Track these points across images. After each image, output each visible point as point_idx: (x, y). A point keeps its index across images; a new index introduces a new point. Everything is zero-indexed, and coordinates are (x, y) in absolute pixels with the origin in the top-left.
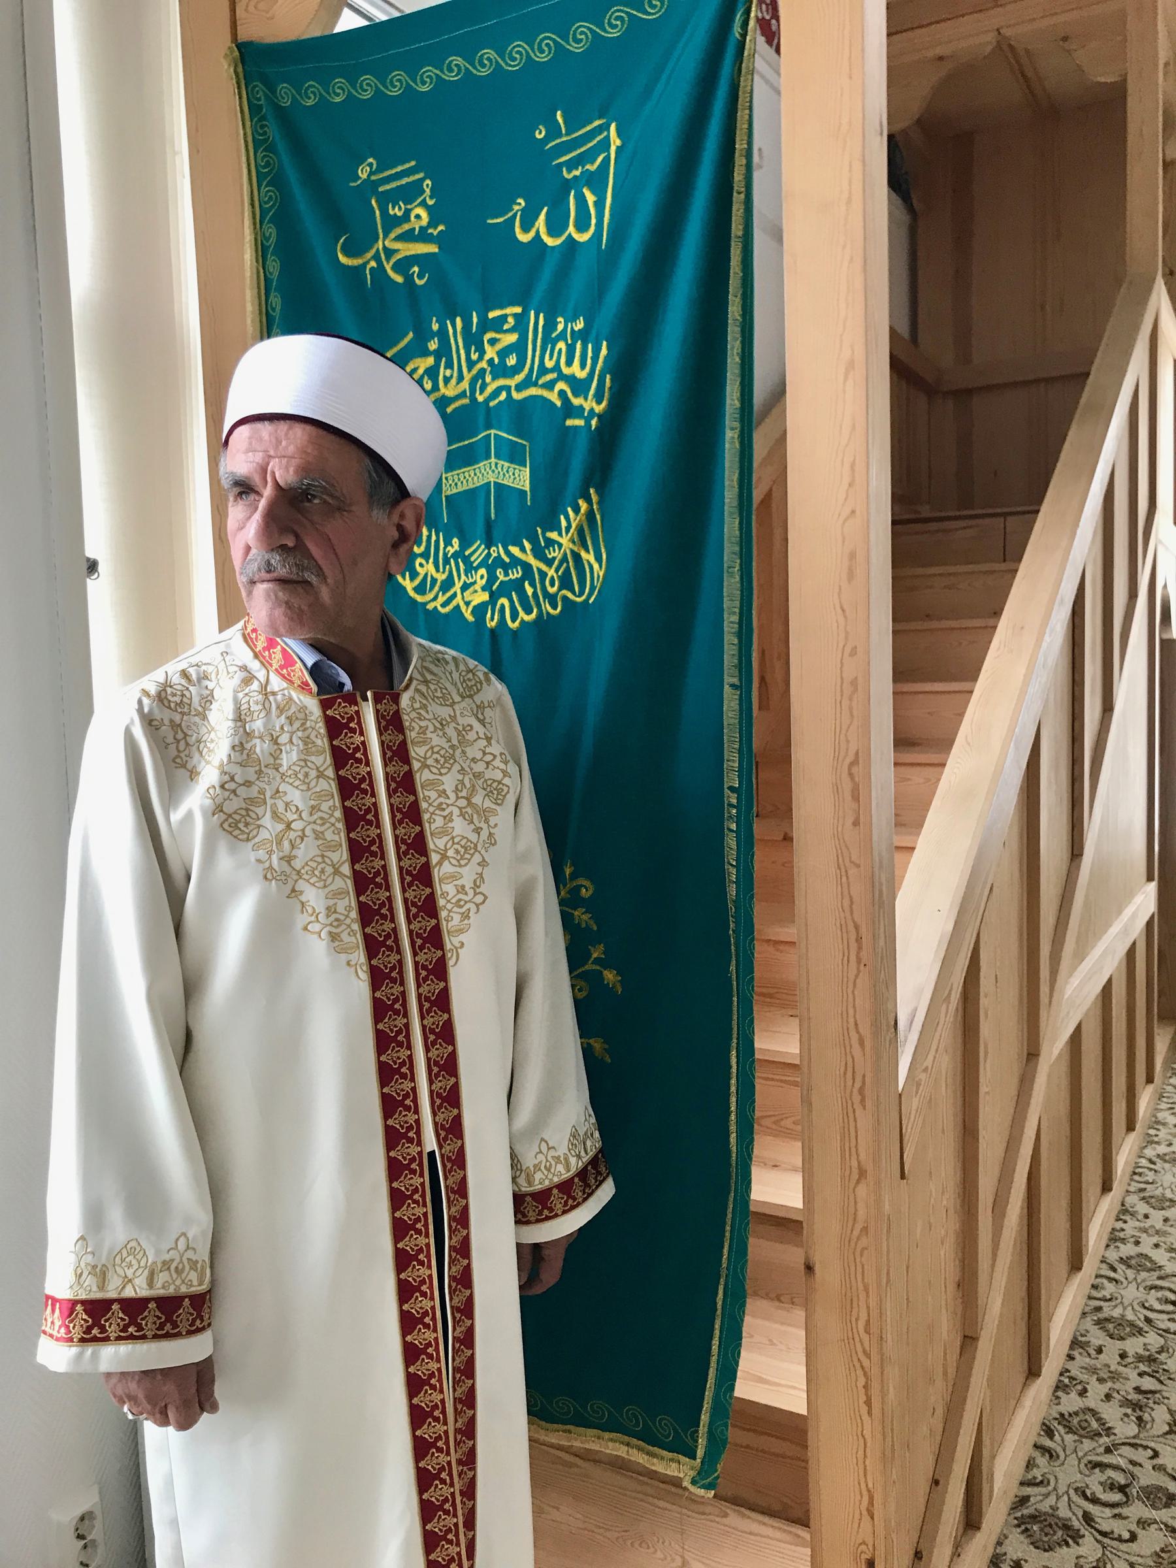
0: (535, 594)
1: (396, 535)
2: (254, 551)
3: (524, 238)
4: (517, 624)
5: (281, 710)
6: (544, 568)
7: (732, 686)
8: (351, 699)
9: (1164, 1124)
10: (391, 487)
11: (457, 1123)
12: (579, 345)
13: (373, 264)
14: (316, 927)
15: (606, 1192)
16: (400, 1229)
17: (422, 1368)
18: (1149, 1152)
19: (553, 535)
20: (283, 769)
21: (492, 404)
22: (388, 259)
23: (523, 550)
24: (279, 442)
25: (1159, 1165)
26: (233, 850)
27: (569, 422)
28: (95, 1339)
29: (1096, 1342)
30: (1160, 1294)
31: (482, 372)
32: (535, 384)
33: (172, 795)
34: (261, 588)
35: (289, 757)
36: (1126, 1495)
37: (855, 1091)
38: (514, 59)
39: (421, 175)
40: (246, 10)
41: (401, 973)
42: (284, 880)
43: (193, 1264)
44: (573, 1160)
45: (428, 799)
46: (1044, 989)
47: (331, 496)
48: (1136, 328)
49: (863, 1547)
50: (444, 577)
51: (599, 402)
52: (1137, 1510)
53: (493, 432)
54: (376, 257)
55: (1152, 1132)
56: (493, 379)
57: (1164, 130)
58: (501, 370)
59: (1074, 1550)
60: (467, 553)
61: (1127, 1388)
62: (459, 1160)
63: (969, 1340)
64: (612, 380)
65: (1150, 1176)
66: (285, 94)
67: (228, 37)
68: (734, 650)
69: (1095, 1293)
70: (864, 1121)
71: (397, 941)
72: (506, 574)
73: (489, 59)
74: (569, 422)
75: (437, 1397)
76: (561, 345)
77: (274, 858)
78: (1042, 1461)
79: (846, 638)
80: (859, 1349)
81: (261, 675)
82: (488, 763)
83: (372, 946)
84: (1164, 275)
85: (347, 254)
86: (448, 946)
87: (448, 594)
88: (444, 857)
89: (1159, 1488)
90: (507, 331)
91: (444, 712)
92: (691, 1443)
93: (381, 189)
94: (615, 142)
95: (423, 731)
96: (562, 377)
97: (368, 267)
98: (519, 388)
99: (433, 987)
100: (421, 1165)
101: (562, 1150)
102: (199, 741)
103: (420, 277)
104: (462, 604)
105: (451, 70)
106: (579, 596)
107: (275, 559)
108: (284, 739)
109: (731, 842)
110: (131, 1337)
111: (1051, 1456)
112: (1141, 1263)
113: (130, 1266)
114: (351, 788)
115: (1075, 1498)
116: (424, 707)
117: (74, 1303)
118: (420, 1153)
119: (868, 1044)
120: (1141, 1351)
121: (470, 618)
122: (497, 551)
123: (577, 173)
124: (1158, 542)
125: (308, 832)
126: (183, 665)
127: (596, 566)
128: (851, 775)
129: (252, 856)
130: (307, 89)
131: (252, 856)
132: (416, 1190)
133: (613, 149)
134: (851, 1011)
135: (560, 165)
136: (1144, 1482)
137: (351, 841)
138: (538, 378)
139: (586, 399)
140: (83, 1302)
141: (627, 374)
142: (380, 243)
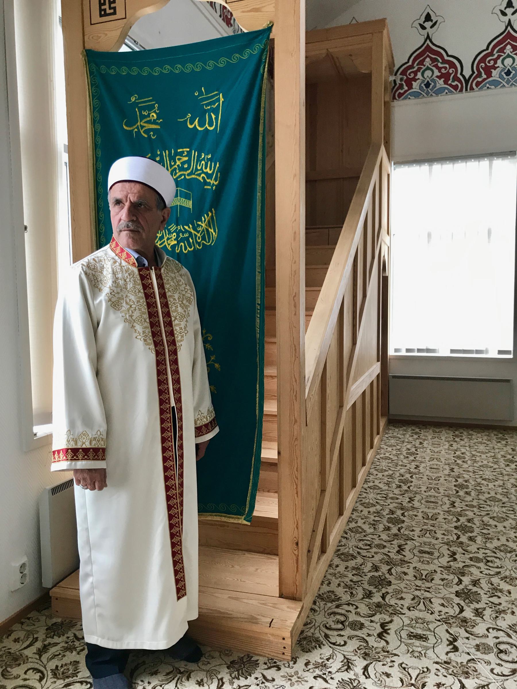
0: (193, 242)
1: (162, 218)
2: (122, 222)
3: (191, 127)
5: (126, 271)
7: (259, 272)
8: (147, 269)
9: (383, 449)
10: (163, 204)
11: (180, 398)
12: (209, 163)
13: (136, 130)
14: (139, 337)
15: (217, 430)
16: (163, 430)
17: (169, 473)
18: (378, 457)
19: (200, 223)
20: (128, 289)
23: (189, 227)
24: (131, 189)
26: (114, 313)
27: (206, 187)
28: (75, 459)
29: (361, 509)
32: (194, 174)
33: (94, 296)
34: (124, 233)
35: (130, 286)
39: (154, 102)
40: (89, 38)
41: (164, 352)
42: (130, 322)
43: (102, 439)
44: (208, 418)
45: (171, 301)
47: (148, 206)
48: (375, 164)
49: (295, 539)
51: (216, 181)
52: (374, 550)
54: (137, 128)
55: (379, 451)
57: (384, 90)
58: (181, 169)
59: (355, 561)
61: (371, 520)
62: (180, 410)
63: (323, 491)
66: (103, 69)
67: (82, 46)
68: (259, 261)
69: (360, 496)
70: (297, 407)
71: (163, 343)
72: (183, 235)
74: (206, 187)
75: (173, 482)
76: (203, 162)
77: (127, 316)
78: (344, 540)
80: (294, 477)
81: (119, 261)
82: (186, 292)
83: (156, 344)
84: (384, 144)
85: (126, 126)
86: (177, 345)
87: (162, 241)
88: (176, 319)
89: (381, 544)
90: (184, 156)
91: (173, 275)
94: (222, 100)
95: (168, 280)
96: (203, 172)
98: (188, 175)
99: (173, 357)
100: (170, 411)
101: (205, 414)
102: (101, 280)
103: (153, 136)
104: (167, 245)
107: (130, 224)
108: (128, 280)
109: (258, 321)
110: (86, 459)
112: (375, 487)
113: (84, 439)
114: (149, 296)
115: (355, 549)
116: (167, 273)
117: (67, 450)
118: (170, 407)
119: (298, 381)
120: (375, 510)
121: (170, 249)
124: (382, 240)
125: (137, 308)
126: (93, 257)
127: (214, 233)
128: (294, 300)
129: (121, 315)
131: (121, 315)
132: (168, 418)
134: (293, 372)
136: (376, 543)
137: (149, 312)
139: (211, 180)
140: (71, 449)
141: (225, 173)
142: (139, 123)
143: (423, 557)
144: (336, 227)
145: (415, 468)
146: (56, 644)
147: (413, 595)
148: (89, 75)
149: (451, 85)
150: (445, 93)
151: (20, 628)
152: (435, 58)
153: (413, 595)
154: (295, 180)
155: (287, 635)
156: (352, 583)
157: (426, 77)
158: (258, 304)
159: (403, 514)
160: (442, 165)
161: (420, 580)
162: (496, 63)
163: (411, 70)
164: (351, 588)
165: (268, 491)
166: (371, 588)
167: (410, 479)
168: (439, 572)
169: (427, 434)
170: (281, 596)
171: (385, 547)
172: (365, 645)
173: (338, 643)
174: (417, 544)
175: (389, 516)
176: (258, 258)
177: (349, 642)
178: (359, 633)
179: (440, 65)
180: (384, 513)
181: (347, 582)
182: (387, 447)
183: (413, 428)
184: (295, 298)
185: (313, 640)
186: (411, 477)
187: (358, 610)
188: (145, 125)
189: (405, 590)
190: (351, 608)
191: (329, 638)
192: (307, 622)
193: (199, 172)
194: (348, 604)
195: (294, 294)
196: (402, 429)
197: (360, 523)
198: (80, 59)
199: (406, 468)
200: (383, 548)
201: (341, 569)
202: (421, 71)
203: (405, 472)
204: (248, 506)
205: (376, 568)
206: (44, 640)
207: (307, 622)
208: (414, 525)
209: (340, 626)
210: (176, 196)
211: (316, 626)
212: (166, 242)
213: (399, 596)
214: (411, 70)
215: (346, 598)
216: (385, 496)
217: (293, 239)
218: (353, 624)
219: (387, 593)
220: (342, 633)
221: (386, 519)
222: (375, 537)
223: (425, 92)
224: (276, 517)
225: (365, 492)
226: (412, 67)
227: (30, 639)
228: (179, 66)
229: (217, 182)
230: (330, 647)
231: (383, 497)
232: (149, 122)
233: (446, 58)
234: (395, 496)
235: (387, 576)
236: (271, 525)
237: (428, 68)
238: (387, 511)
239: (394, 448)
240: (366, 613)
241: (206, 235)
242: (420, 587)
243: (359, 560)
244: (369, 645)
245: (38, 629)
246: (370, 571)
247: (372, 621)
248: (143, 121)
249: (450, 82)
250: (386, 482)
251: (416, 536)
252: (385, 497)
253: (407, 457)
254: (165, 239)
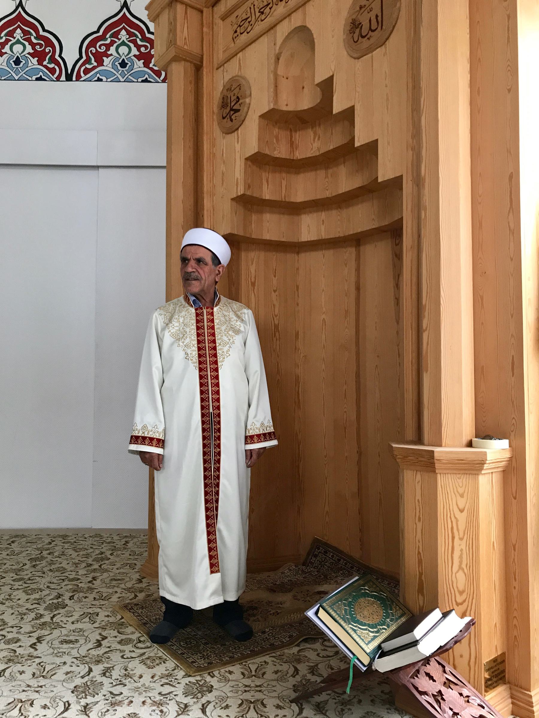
15: (274, 442)
86: (219, 365)
149: (46, 67)
157: (121, 54)
162: (108, 49)
166: (188, 700)
168: (270, 663)
179: (140, 43)
223: (120, 73)
226: (103, 38)
233: (42, 33)
249: (45, 63)
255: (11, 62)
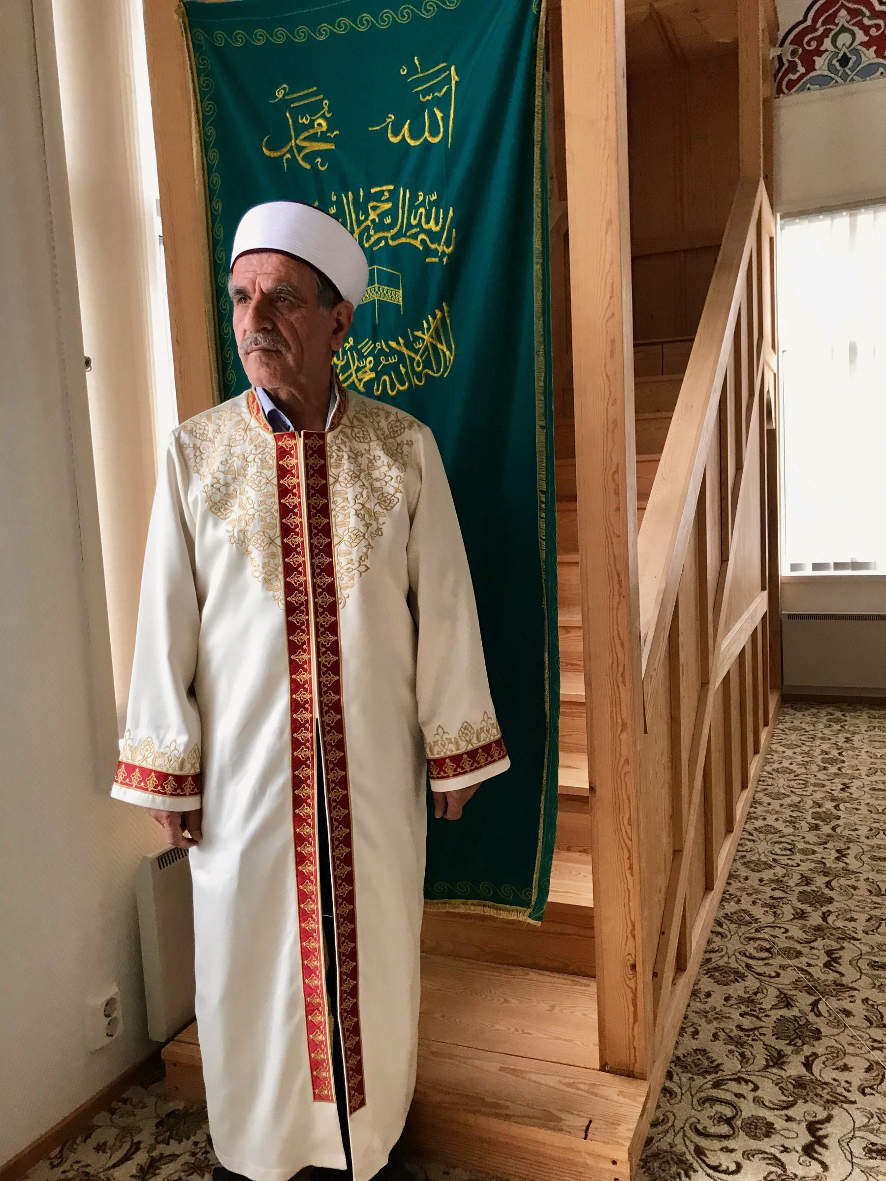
0: (407, 372)
1: (335, 325)
2: (248, 332)
3: (394, 140)
4: (394, 392)
6: (412, 355)
7: (541, 427)
9: (776, 752)
10: (331, 295)
12: (434, 211)
13: (288, 156)
18: (768, 768)
19: (419, 334)
21: (374, 249)
22: (299, 153)
25: (775, 775)
27: (428, 260)
29: (744, 874)
30: (781, 846)
31: (368, 228)
32: (405, 236)
36: (771, 953)
37: (619, 675)
38: (384, 21)
39: (321, 97)
46: (711, 642)
49: (629, 957)
50: (343, 363)
51: (448, 247)
52: (779, 960)
53: (375, 267)
55: (769, 756)
56: (375, 233)
58: (380, 226)
60: (359, 347)
63: (677, 852)
64: (456, 233)
65: (770, 782)
66: (220, 38)
69: (740, 848)
72: (387, 360)
73: (366, 20)
74: (428, 260)
76: (422, 210)
78: (717, 939)
79: (610, 394)
85: (269, 149)
87: (346, 375)
89: (790, 948)
90: (383, 201)
92: (525, 898)
93: (292, 106)
94: (455, 78)
96: (423, 231)
97: (285, 158)
98: (393, 238)
103: (322, 165)
104: (356, 381)
105: (340, 27)
106: (437, 373)
107: (260, 337)
109: (542, 524)
111: (722, 936)
112: (769, 830)
115: (740, 957)
122: (381, 345)
123: (429, 98)
124: (765, 361)
127: (448, 353)
128: (614, 480)
130: (237, 34)
133: (453, 82)
134: (615, 626)
135: (417, 92)
138: (406, 231)
139: (439, 245)
141: (465, 229)
142: (293, 142)
143: (879, 976)
144: (681, 341)
145: (842, 789)
146: (174, 1157)
147: (868, 1060)
148: (192, 50)
150: (879, 73)
151: (109, 1123)
152: (855, 9)
153: (868, 1060)
154: (610, 233)
155: (622, 1155)
156: (742, 1034)
158: (542, 492)
159: (828, 885)
160: (875, 212)
161: (878, 1026)
163: (810, 36)
164: (740, 1044)
165: (569, 849)
166: (781, 1045)
167: (834, 811)
169: (857, 721)
170: (603, 1069)
171: (799, 954)
172: (780, 1172)
173: (724, 1167)
174: (865, 949)
175: (801, 889)
176: (539, 397)
177: (745, 1164)
178: (764, 1145)
179: (866, 22)
180: (791, 883)
181: (731, 1031)
182: (783, 749)
183: (830, 710)
184: (616, 476)
185: (672, 1159)
186: (837, 807)
187: (759, 1093)
188: (305, 144)
189: (850, 1049)
190: (745, 1089)
191: (705, 1155)
192: (658, 1119)
193: (414, 231)
194: (739, 1080)
195: (614, 468)
196: (809, 712)
197: (746, 903)
198: (175, 20)
199: (824, 789)
200: (797, 957)
201: (716, 1001)
202: (831, 36)
203: (823, 798)
204: (535, 891)
205: (786, 1001)
206: (152, 1148)
207: (658, 1119)
208: (853, 908)
209: (724, 1129)
210: (371, 282)
211: (677, 1129)
212: (354, 375)
213: (840, 1064)
214: (810, 36)
215: (731, 1065)
216: (789, 847)
217: (608, 355)
218: (750, 1125)
219: (815, 1055)
220: (731, 1144)
221: (796, 893)
222: (777, 932)
224: (591, 904)
225: (750, 840)
226: (812, 28)
227: (126, 1146)
228: (367, 16)
229: (451, 248)
230: (709, 1175)
231: (785, 849)
232: (313, 138)
234: (808, 846)
235: (811, 1017)
236: (580, 919)
237: (844, 29)
238: (796, 878)
239: (798, 750)
240: (776, 1102)
241: (432, 356)
242: (879, 1042)
243: (752, 982)
244: (788, 1172)
245: (141, 1125)
246: (774, 1007)
247: (789, 1119)
248: (302, 137)
250: (789, 819)
251: (860, 931)
252: (790, 850)
253: (825, 768)
254: (353, 370)
255: (835, 62)
